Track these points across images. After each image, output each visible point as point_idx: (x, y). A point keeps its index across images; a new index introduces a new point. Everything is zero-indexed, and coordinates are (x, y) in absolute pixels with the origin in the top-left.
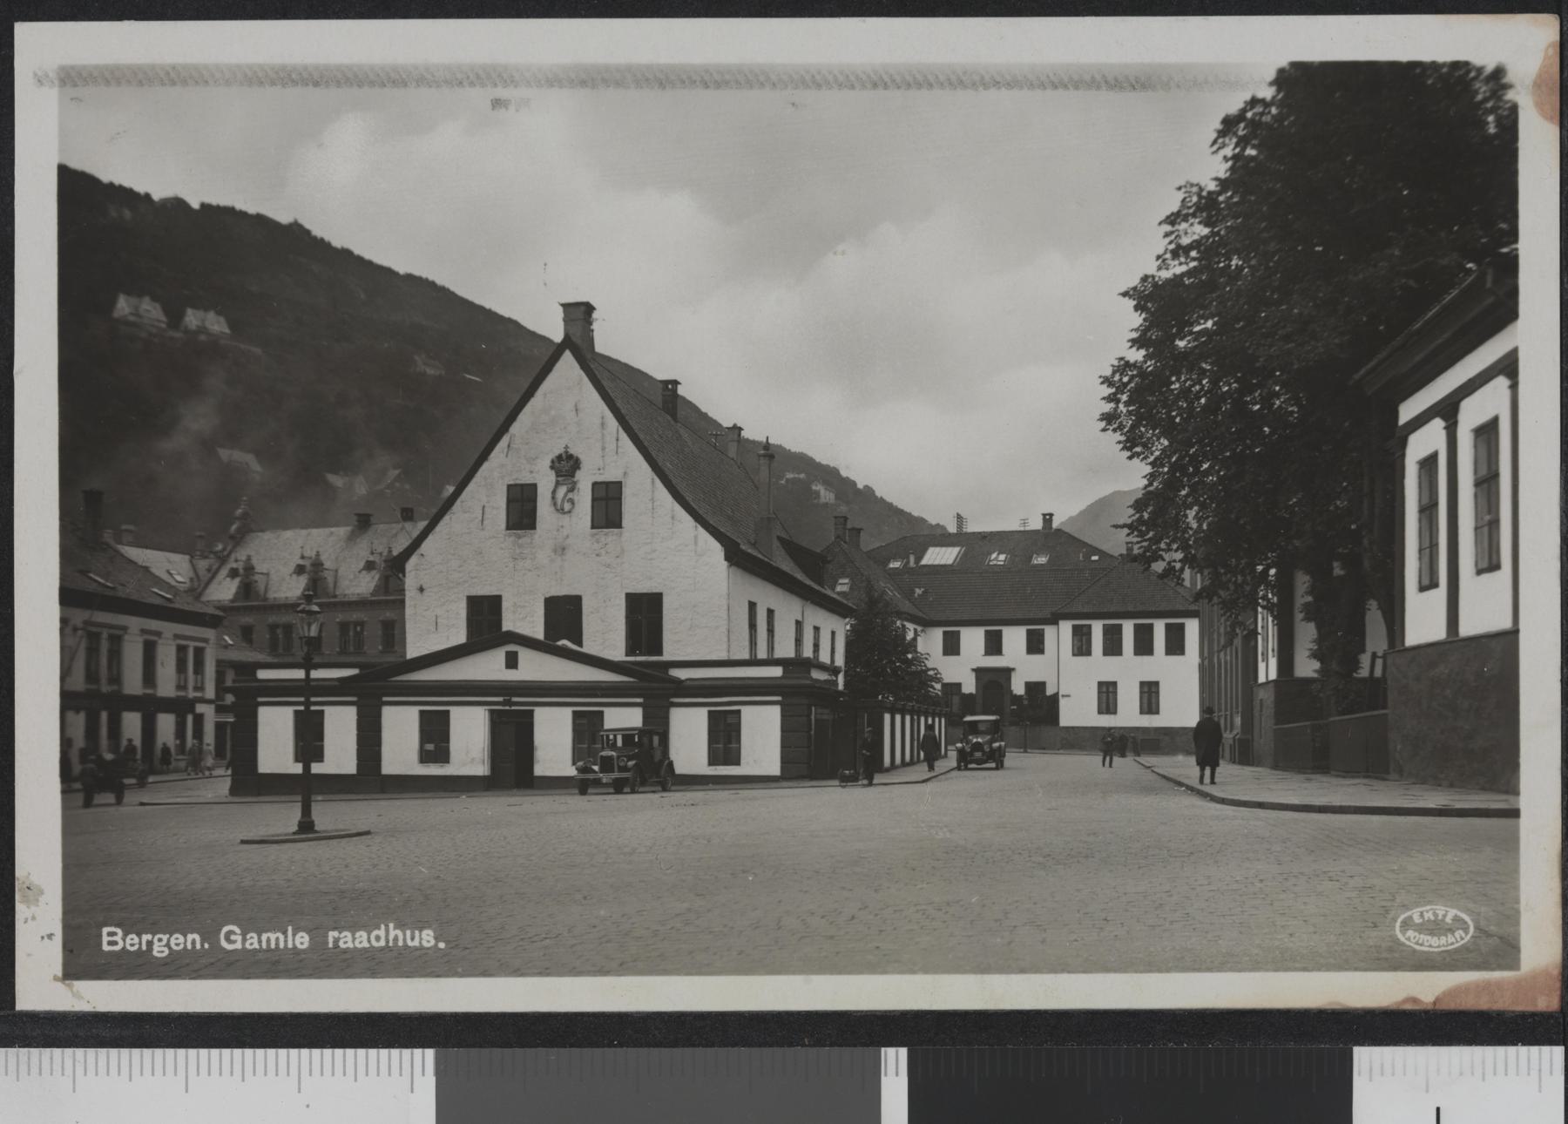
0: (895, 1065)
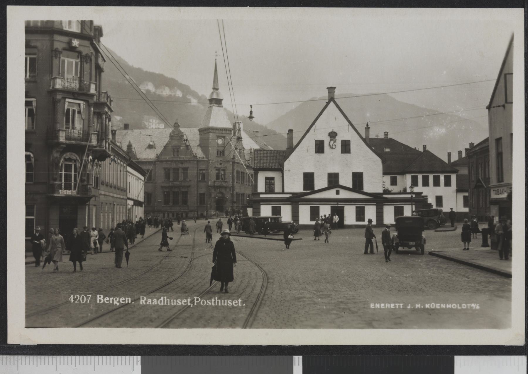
0: (298, 361)
